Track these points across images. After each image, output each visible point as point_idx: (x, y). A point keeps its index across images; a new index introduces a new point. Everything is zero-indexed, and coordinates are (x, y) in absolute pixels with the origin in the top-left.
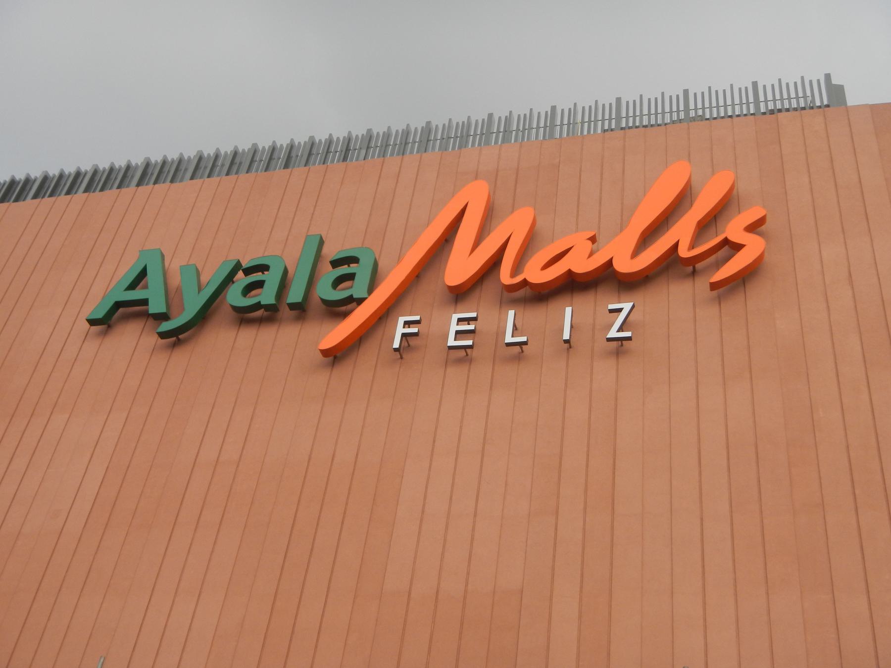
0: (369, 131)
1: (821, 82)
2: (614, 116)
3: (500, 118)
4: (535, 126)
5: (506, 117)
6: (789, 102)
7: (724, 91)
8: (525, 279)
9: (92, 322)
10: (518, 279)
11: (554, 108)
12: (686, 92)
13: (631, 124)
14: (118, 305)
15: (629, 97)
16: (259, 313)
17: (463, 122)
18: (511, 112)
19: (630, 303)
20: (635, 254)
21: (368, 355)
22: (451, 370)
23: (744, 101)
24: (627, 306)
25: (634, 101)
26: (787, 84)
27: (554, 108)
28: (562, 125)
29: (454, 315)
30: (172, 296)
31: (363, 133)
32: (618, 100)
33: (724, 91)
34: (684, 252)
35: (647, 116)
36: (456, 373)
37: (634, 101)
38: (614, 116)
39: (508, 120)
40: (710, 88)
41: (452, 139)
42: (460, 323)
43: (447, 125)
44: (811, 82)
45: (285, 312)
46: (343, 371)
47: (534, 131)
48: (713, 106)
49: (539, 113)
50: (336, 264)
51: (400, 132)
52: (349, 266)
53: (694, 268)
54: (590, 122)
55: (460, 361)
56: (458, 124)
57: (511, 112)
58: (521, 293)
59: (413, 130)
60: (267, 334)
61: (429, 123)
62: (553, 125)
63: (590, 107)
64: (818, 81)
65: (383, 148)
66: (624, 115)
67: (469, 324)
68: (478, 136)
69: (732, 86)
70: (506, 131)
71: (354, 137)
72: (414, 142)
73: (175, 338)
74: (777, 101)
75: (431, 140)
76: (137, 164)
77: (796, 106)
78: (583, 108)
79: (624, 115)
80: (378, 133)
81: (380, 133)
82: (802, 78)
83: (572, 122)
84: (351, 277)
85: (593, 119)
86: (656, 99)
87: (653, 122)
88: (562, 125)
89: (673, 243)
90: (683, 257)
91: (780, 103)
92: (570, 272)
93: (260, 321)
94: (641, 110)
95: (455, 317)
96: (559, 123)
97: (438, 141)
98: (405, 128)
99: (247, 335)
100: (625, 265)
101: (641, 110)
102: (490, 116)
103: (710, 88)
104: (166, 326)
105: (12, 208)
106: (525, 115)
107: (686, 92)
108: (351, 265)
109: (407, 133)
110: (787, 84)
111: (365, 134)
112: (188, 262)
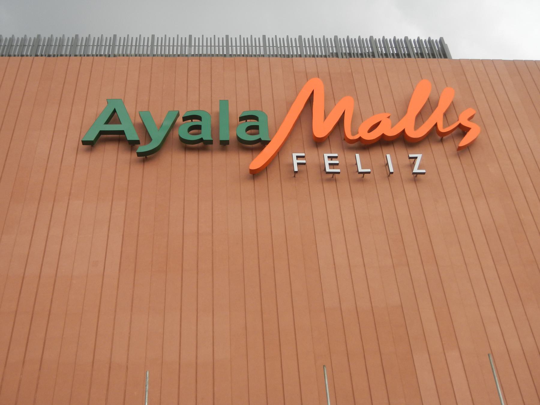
2: (225, 45)
3: (82, 38)
4: (130, 44)
5: (87, 38)
6: (177, 48)
7: (174, 38)
8: (360, 137)
9: (84, 143)
10: (356, 137)
11: (115, 36)
13: (133, 53)
14: (101, 133)
15: (159, 35)
16: (201, 144)
18: (89, 35)
20: (416, 127)
21: (274, 174)
22: (326, 185)
23: (242, 45)
24: (419, 156)
26: (255, 38)
27: (115, 36)
28: (119, 46)
29: (293, 154)
30: (143, 129)
32: (153, 36)
33: (174, 38)
34: (441, 129)
35: (134, 47)
36: (329, 187)
39: (88, 40)
40: (178, 35)
41: (41, 46)
42: (298, 159)
43: (100, 38)
44: (244, 38)
45: (216, 144)
46: (261, 183)
47: (129, 47)
48: (224, 45)
49: (120, 38)
50: (185, 119)
52: (246, 121)
53: (442, 138)
54: (161, 46)
55: (329, 180)
57: (89, 35)
58: (356, 144)
59: (28, 39)
60: (205, 158)
61: (77, 36)
62: (114, 45)
63: (162, 38)
65: (9, 47)
66: (155, 44)
67: (331, 160)
68: (125, 47)
70: (86, 46)
72: (29, 45)
73: (145, 157)
74: (186, 47)
75: (26, 46)
77: (235, 54)
78: (94, 38)
79: (155, 44)
80: (30, 38)
81: (388, 39)
82: (165, 36)
83: (15, 45)
84: (199, 127)
85: (138, 45)
87: (145, 53)
88: (119, 46)
89: (378, 121)
90: (443, 132)
91: (134, 48)
92: (383, 135)
93: (198, 150)
94: (195, 48)
95: (326, 156)
96: (118, 44)
97: (57, 47)
98: (23, 37)
99: (192, 158)
100: (412, 134)
101: (195, 48)
103: (178, 35)
104: (142, 149)
108: (248, 120)
109: (24, 40)
111: (36, 38)
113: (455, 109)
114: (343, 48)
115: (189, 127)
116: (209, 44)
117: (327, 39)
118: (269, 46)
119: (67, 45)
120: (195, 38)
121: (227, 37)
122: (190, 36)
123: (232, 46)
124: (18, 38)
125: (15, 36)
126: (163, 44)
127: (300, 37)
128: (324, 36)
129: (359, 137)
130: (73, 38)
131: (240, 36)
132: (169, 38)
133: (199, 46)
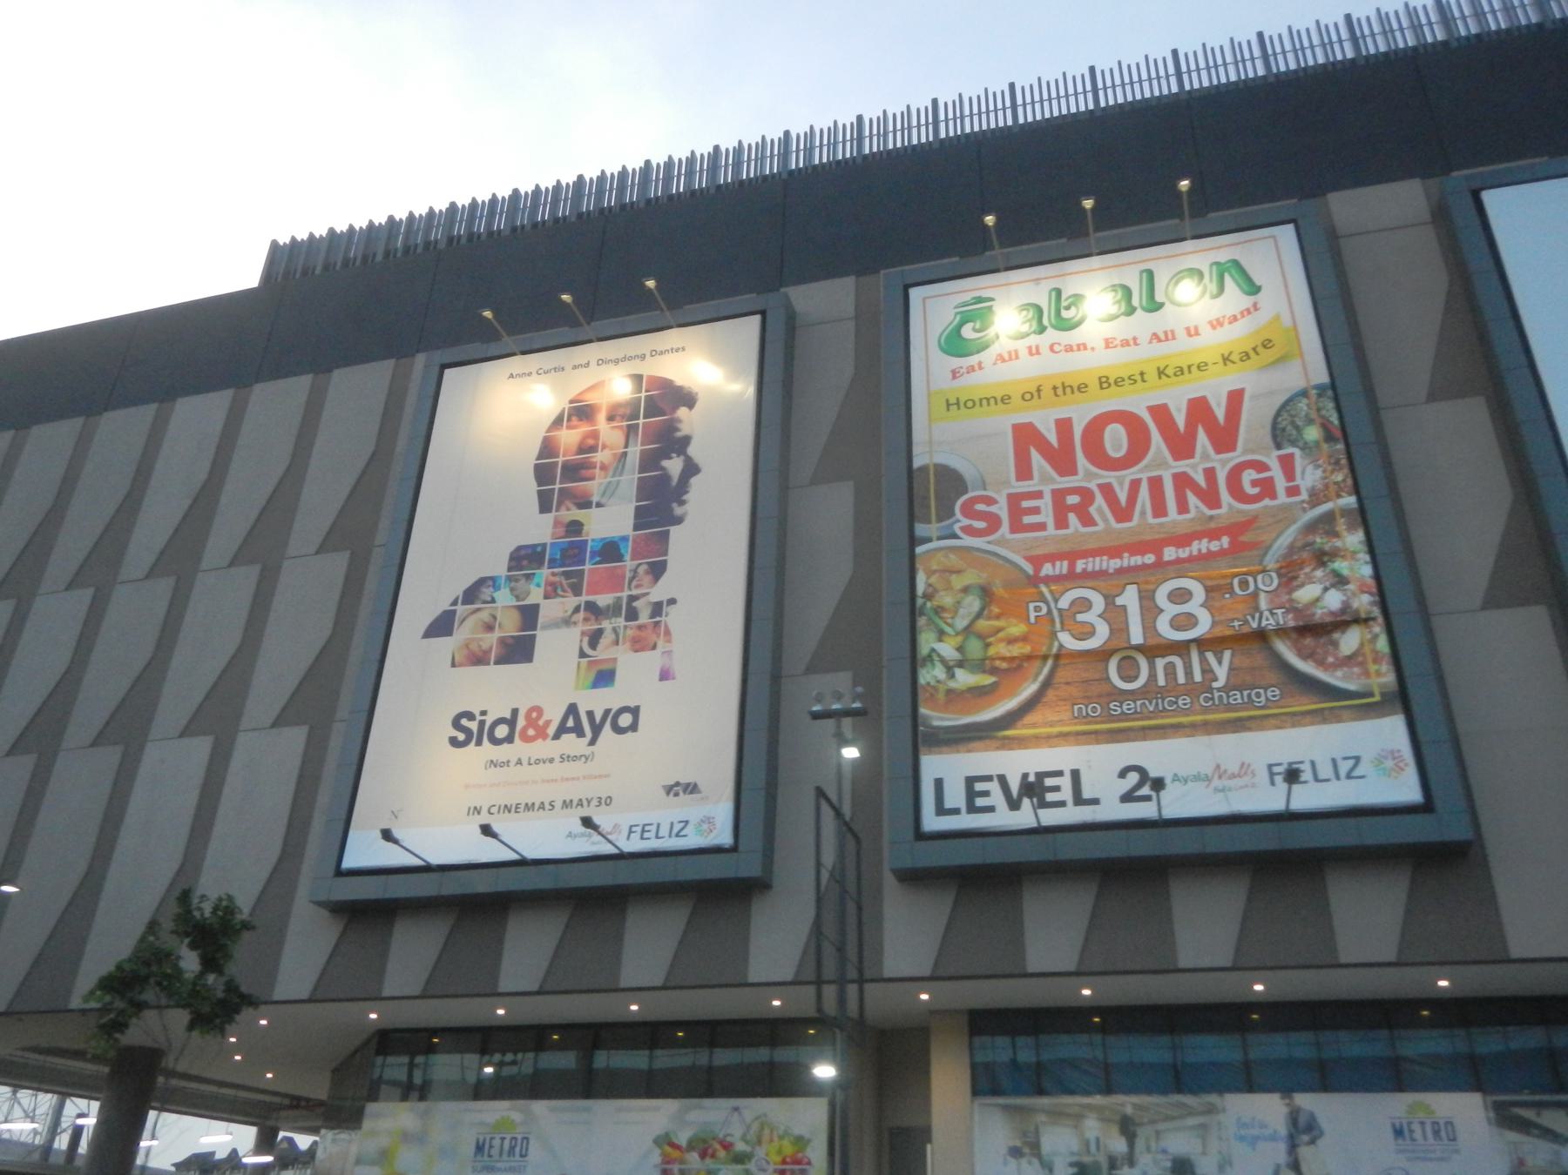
0: (516, 191)
1: (1167, 61)
12: (1012, 86)
17: (757, 144)
19: (76, 420)
25: (979, 97)
28: (947, 120)
31: (902, 110)
33: (1111, 70)
37: (979, 97)
38: (930, 120)
51: (638, 170)
56: (750, 146)
59: (609, 176)
64: (1249, 42)
69: (1064, 74)
71: (544, 190)
76: (401, 220)
86: (1057, 81)
94: (1190, 77)
101: (1190, 77)
102: (787, 133)
105: (1304, 1168)
106: (878, 118)
107: (1012, 86)
110: (1212, 49)
112: (83, 443)
113: (1102, 269)
114: (1398, 34)
115: (193, 1152)
116: (1127, 80)
117: (1415, 8)
118: (1189, 72)
119: (701, 170)
120: (1103, 72)
121: (1260, 35)
122: (1175, 53)
123: (1275, 54)
124: (634, 170)
125: (540, 185)
126: (1211, 64)
127: (1348, 17)
128: (1318, 22)
129: (598, 649)
130: (780, 139)
131: (1204, 45)
132: (1129, 66)
133: (1123, 85)
